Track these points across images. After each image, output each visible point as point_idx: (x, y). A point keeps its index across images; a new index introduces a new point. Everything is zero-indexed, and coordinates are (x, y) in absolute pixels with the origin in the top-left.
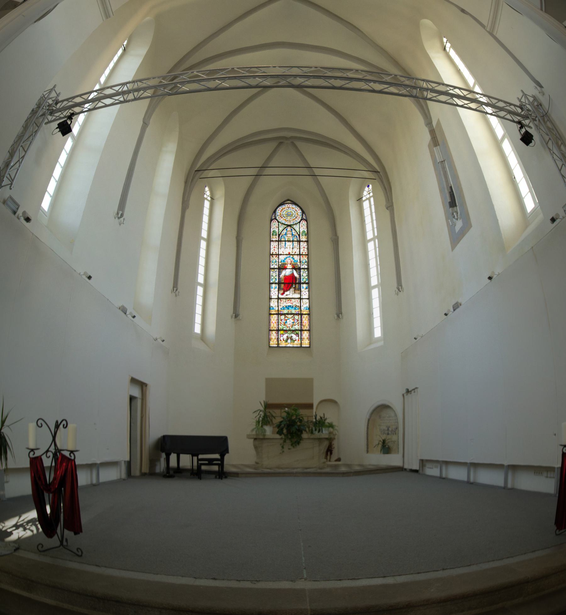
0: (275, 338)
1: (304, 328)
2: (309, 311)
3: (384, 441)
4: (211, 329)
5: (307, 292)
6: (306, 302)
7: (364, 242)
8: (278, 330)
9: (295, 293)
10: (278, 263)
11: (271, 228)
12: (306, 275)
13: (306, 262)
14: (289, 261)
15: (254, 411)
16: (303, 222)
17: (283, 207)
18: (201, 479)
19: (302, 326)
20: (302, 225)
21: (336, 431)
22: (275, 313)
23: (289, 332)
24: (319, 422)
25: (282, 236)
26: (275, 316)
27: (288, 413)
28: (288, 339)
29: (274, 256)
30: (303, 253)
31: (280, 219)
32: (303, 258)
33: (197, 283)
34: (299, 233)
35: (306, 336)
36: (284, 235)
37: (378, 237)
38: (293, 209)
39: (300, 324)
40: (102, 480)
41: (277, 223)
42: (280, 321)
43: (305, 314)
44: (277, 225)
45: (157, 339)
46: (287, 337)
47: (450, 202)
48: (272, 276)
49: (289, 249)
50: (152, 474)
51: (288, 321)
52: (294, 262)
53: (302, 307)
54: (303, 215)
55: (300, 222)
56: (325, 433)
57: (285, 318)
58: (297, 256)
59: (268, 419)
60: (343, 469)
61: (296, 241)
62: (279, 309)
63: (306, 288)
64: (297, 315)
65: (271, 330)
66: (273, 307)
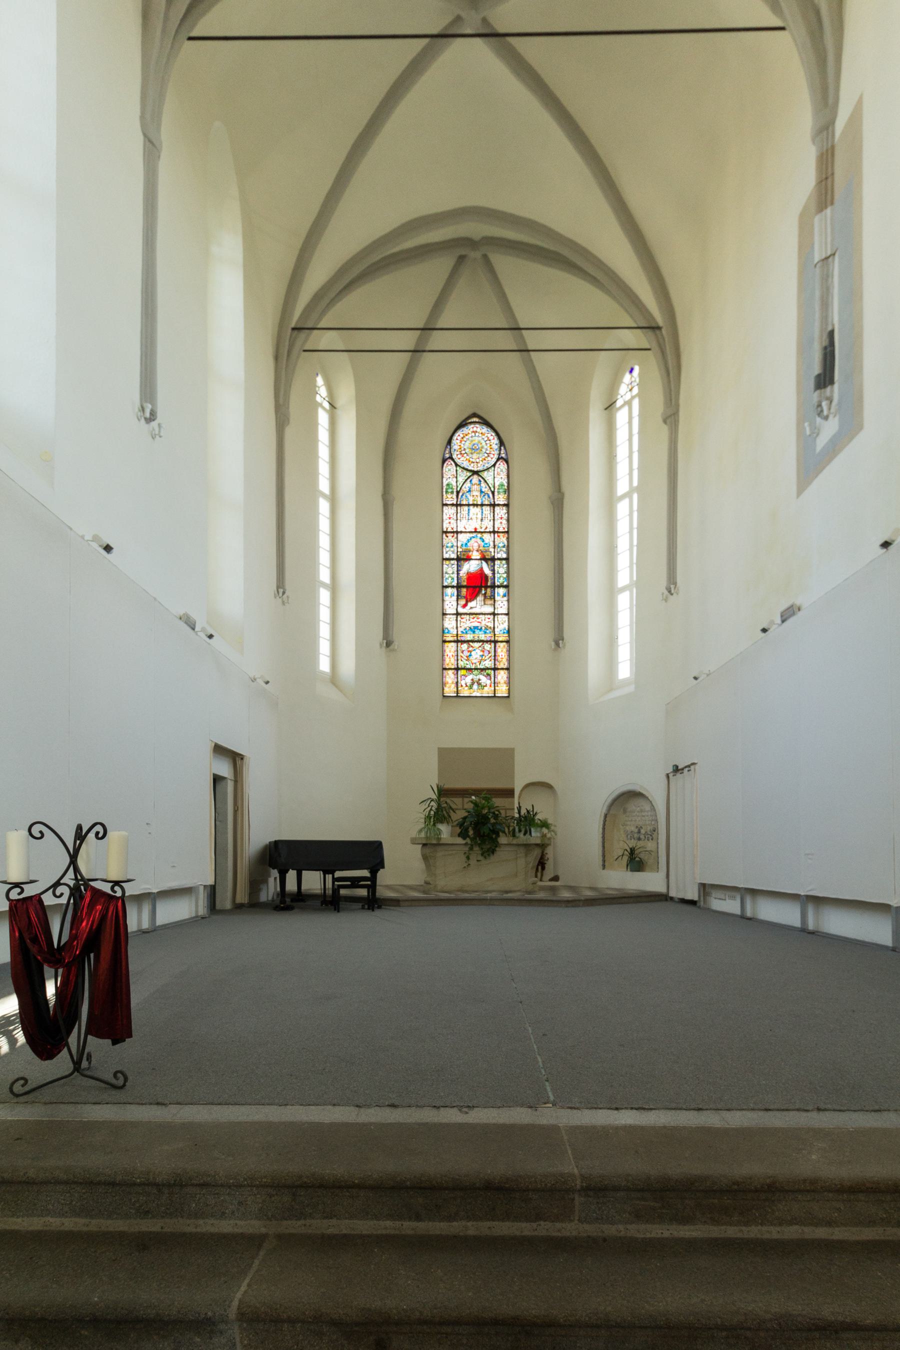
0: (453, 683)
1: (500, 664)
2: (509, 636)
3: (632, 851)
4: (348, 666)
5: (506, 603)
6: (504, 620)
7: (610, 500)
9: (485, 604)
10: (456, 548)
11: (442, 477)
12: (504, 572)
13: (504, 547)
14: (476, 545)
15: (421, 801)
16: (502, 463)
17: (465, 430)
18: (339, 911)
19: (496, 662)
20: (499, 470)
21: (553, 833)
22: (452, 639)
23: (476, 672)
24: (525, 817)
25: (463, 495)
26: (453, 644)
27: (476, 804)
28: (473, 684)
29: (450, 535)
30: (499, 529)
31: (459, 459)
32: (499, 539)
33: (318, 582)
34: (492, 489)
35: (502, 678)
36: (467, 492)
37: (638, 489)
38: (483, 437)
39: (493, 658)
40: (161, 920)
41: (455, 468)
42: (460, 654)
43: (502, 642)
44: (455, 471)
45: (255, 679)
46: (472, 680)
47: (819, 376)
48: (446, 573)
49: (475, 521)
50: (253, 905)
51: (473, 653)
52: (484, 547)
53: (496, 630)
54: (500, 450)
55: (494, 465)
56: (536, 835)
57: (468, 648)
58: (489, 534)
59: (444, 812)
60: (566, 895)
61: (487, 505)
62: (459, 633)
63: (504, 596)
64: (489, 643)
65: (445, 669)
66: (449, 629)
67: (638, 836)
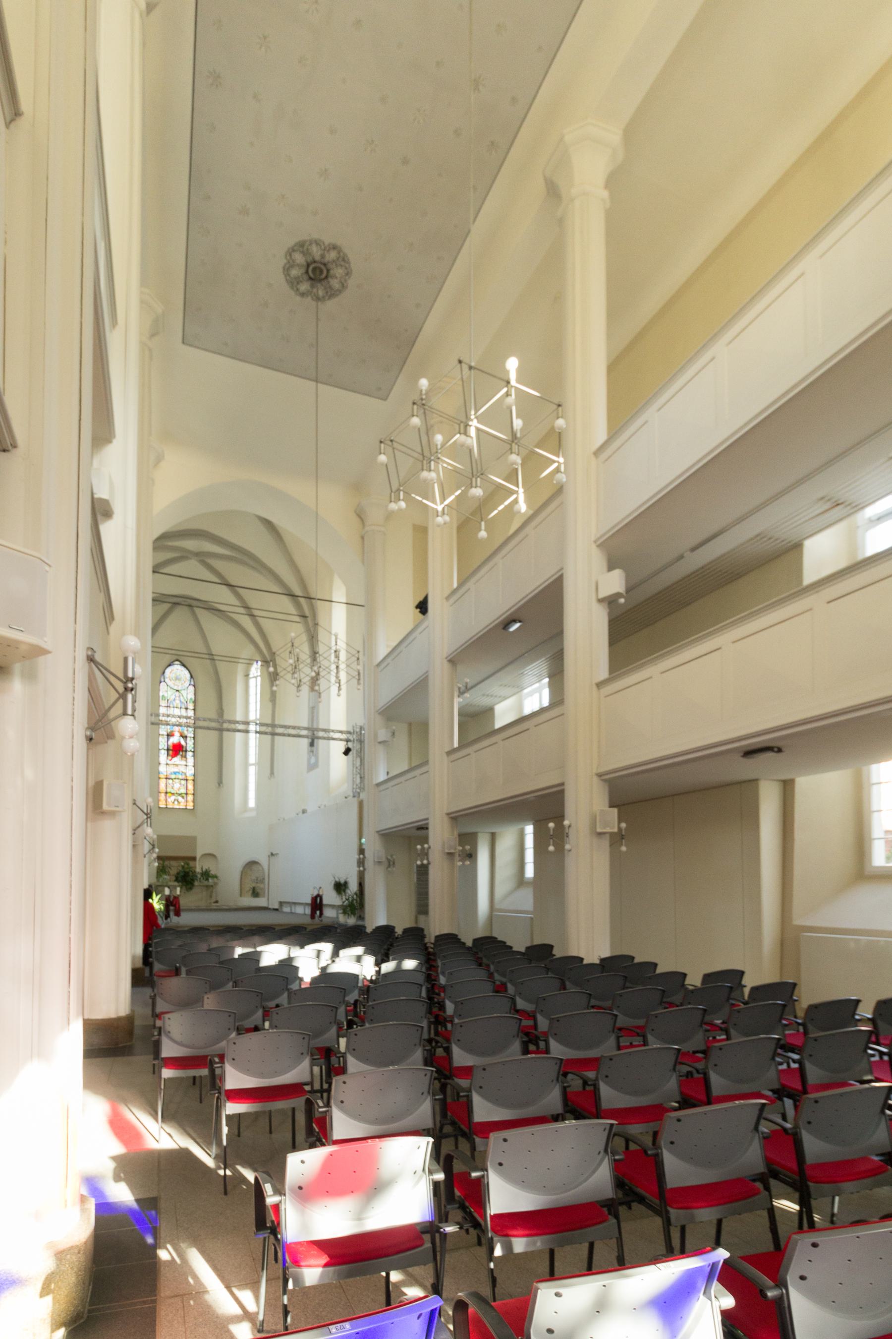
8: (166, 793)
27: (183, 867)
67: (337, 275)
